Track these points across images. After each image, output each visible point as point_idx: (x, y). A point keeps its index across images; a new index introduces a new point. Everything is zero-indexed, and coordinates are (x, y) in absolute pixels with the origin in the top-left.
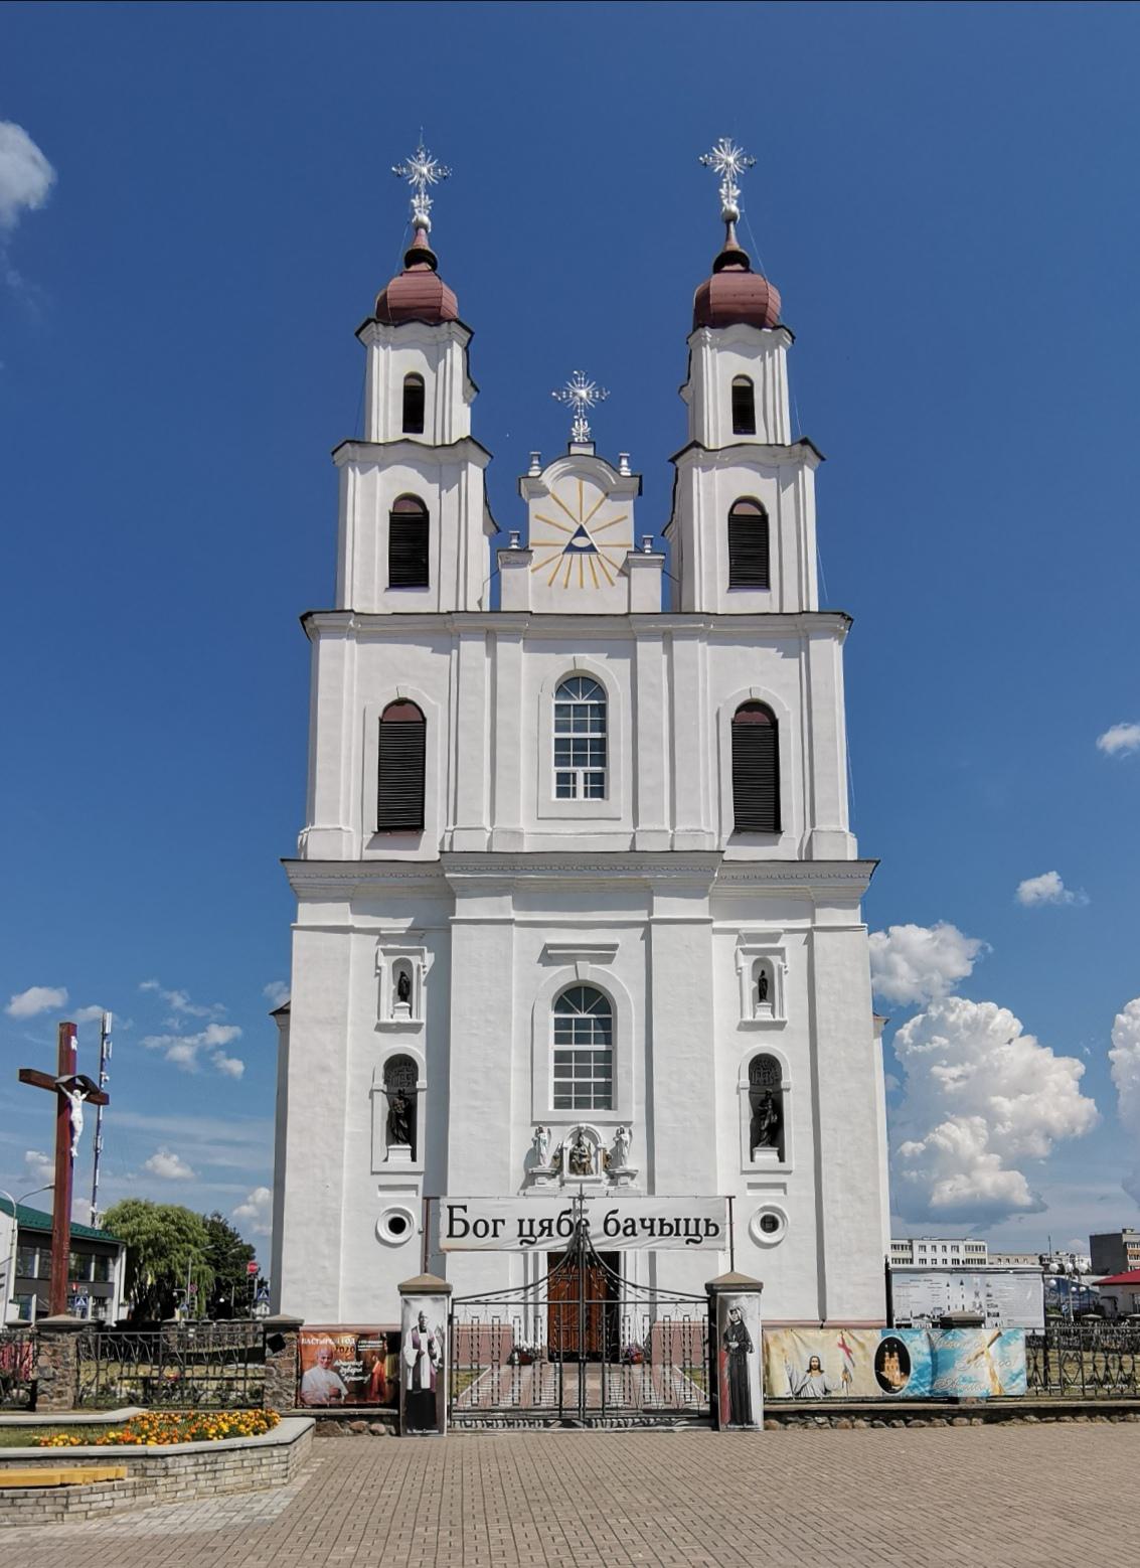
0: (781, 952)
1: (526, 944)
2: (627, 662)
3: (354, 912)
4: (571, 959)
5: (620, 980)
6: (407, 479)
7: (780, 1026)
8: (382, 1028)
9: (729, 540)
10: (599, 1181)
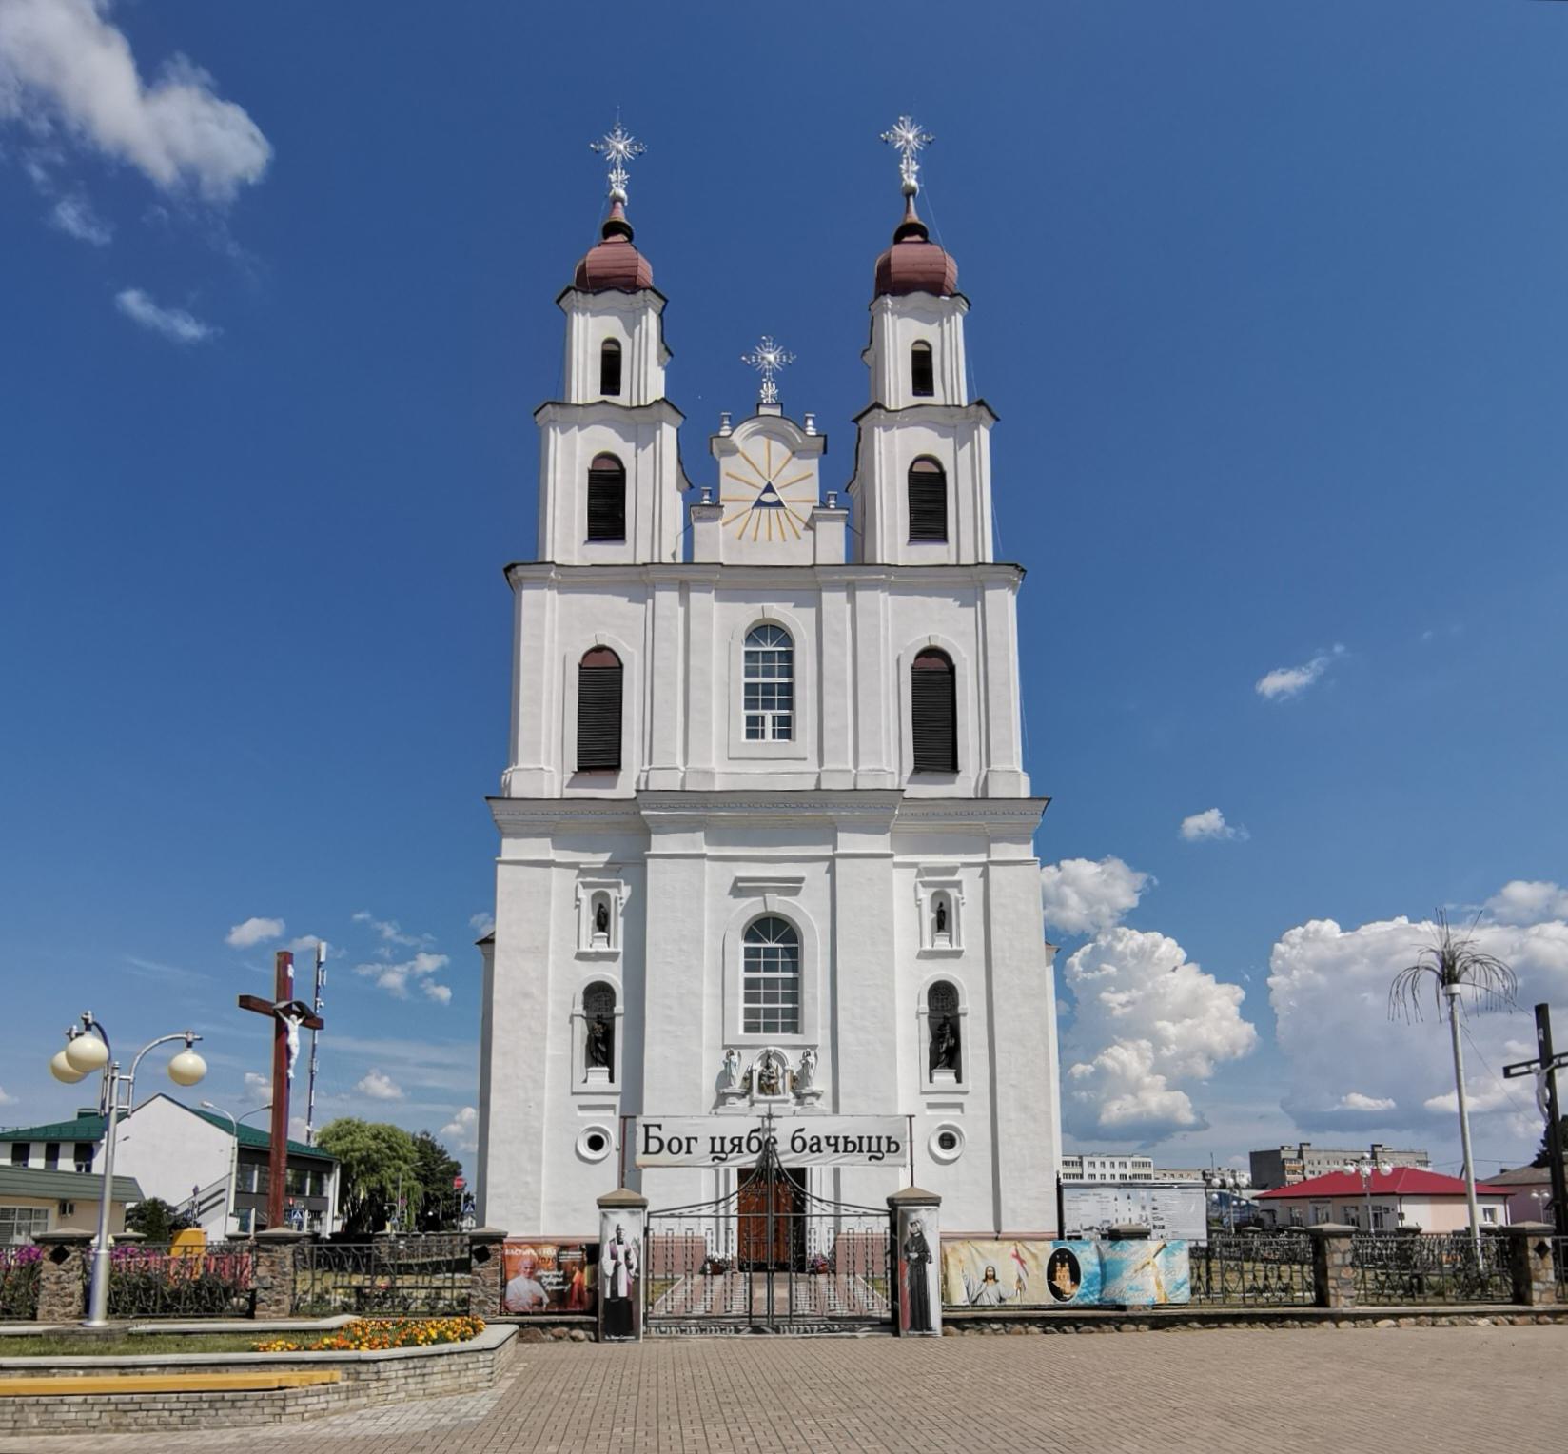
0: (958, 884)
1: (717, 877)
2: (813, 611)
4: (760, 892)
5: (806, 911)
6: (606, 439)
7: (957, 954)
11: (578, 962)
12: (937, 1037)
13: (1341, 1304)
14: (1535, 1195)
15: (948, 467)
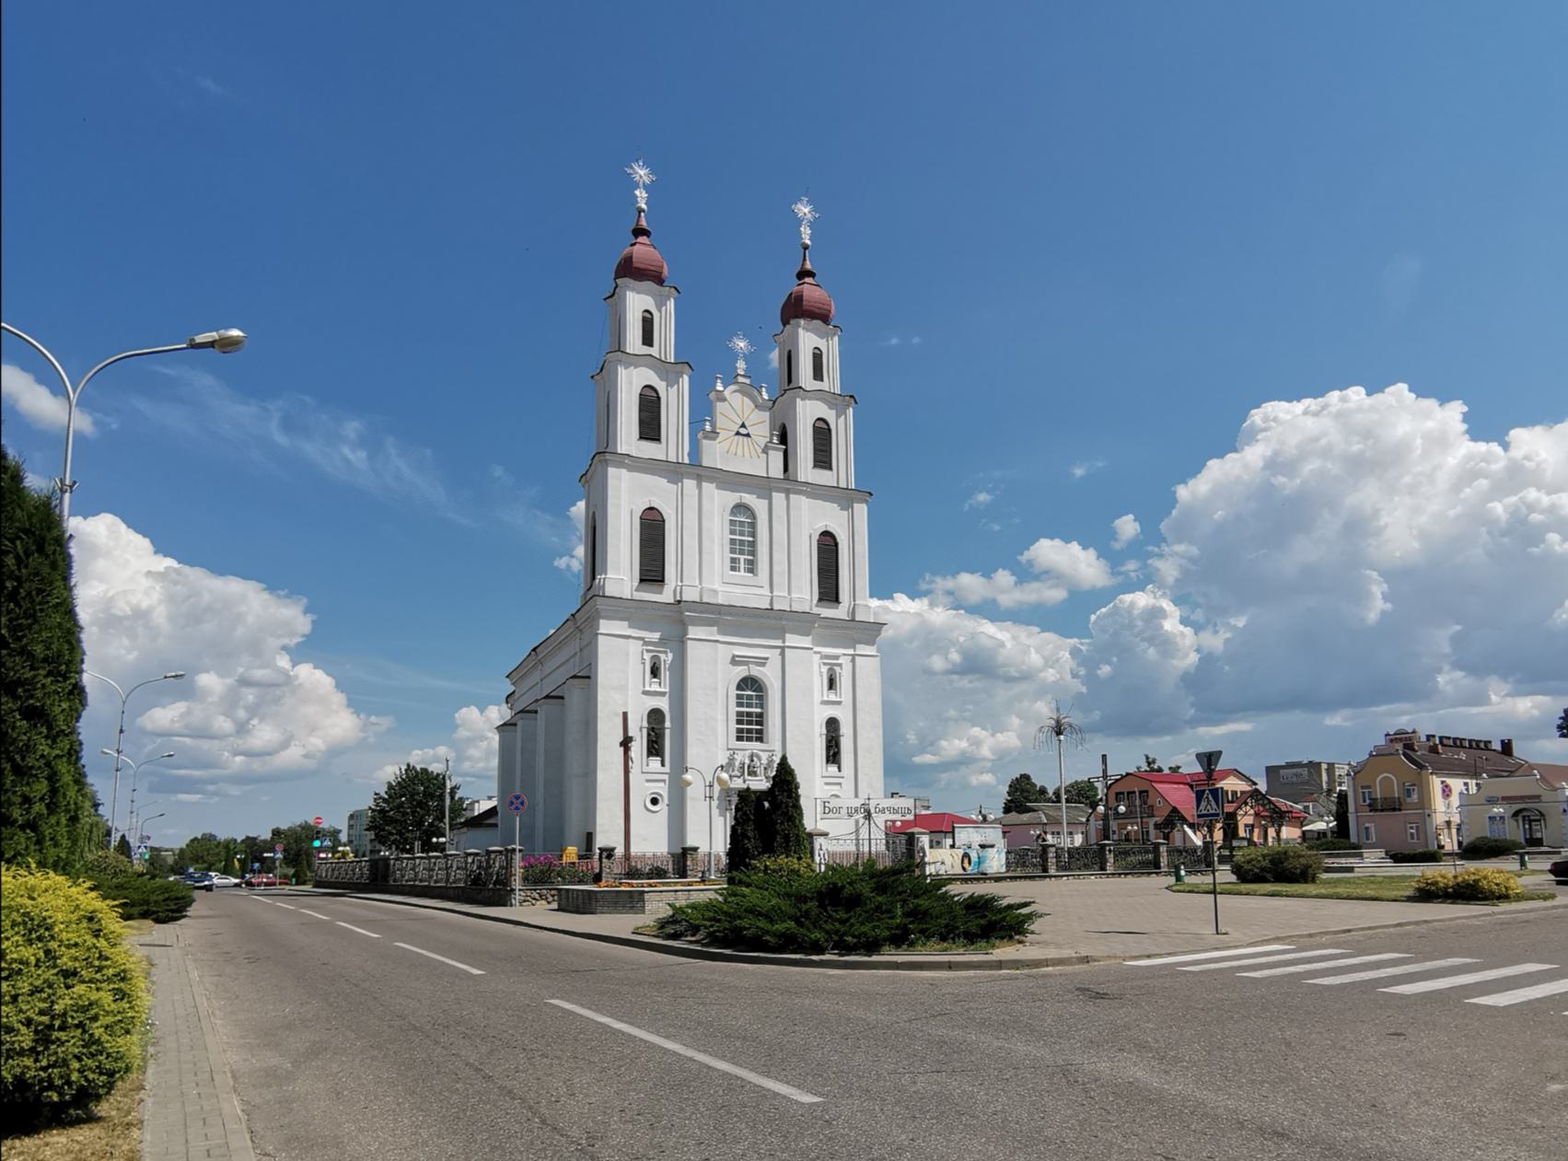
0: (840, 665)
1: (724, 653)
2: (766, 501)
3: (630, 627)
4: (746, 663)
5: (769, 675)
6: (646, 376)
7: (839, 703)
8: (645, 693)
9: (814, 440)
10: (762, 780)
11: (643, 696)
12: (828, 748)
13: (1052, 871)
14: (1032, 832)
15: (833, 427)
